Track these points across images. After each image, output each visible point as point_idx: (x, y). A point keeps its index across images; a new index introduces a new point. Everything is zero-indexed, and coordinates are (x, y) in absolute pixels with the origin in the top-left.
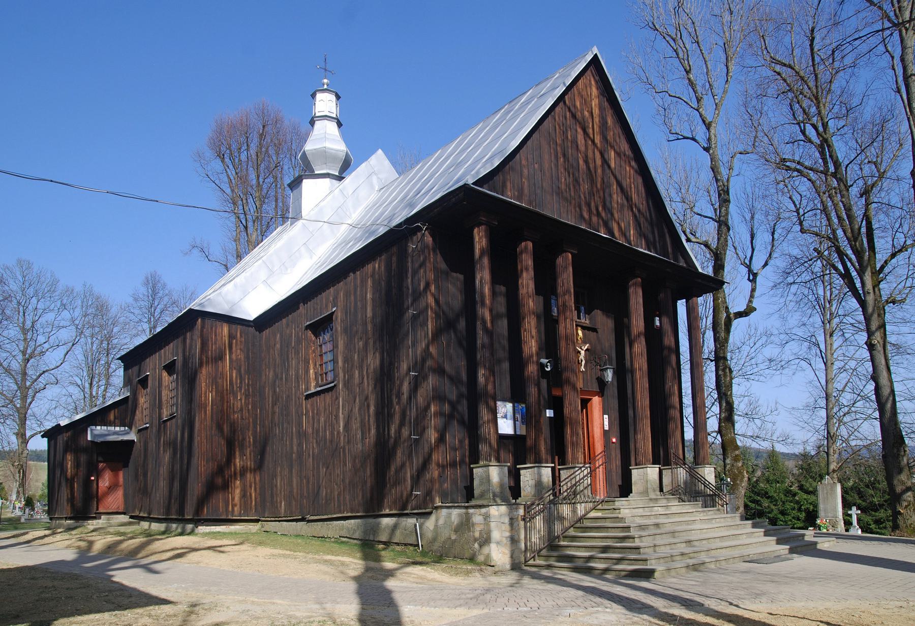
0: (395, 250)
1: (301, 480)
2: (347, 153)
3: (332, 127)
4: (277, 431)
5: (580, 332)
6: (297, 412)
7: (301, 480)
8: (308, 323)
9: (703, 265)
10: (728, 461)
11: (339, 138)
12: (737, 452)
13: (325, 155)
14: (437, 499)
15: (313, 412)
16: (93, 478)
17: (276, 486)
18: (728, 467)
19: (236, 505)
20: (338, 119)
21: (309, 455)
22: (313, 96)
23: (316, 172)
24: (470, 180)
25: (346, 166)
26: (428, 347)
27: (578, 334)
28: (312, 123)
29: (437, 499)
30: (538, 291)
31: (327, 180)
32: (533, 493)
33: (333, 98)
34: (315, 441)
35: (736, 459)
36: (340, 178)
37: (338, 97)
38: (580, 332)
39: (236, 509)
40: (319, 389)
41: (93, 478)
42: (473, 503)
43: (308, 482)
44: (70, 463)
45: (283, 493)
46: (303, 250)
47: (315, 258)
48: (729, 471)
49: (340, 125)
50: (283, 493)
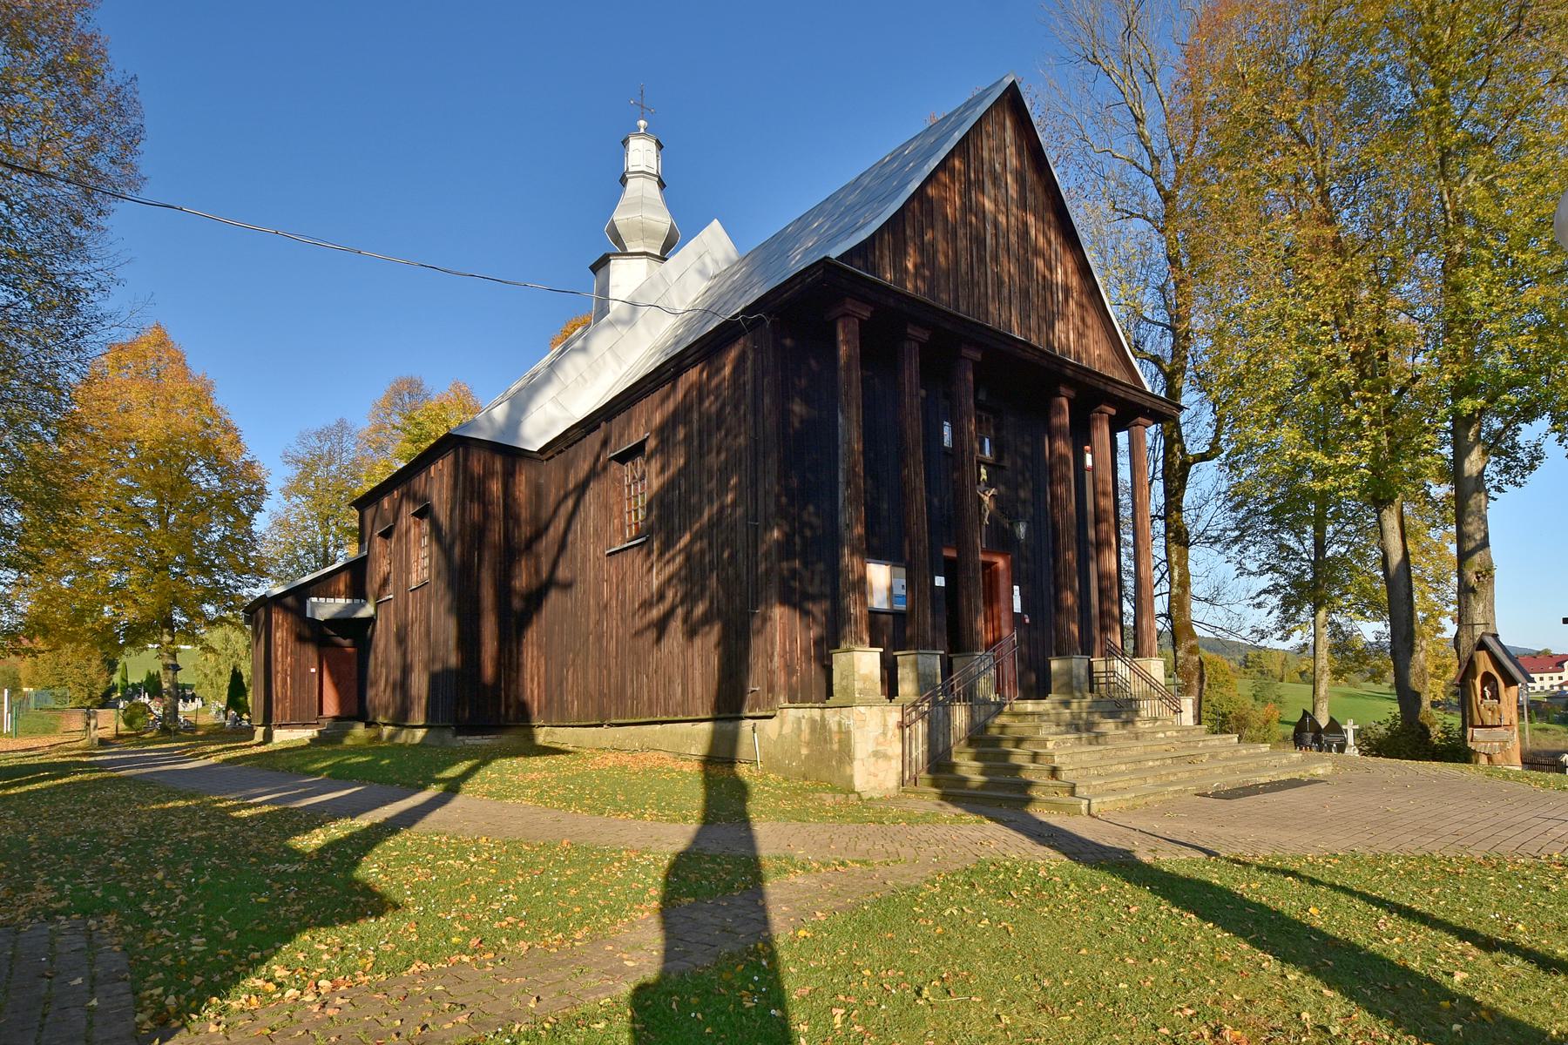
0: (1071, 556)
1: (600, 672)
2: (672, 225)
3: (652, 187)
4: (569, 605)
5: (983, 471)
6: (596, 577)
7: (600, 672)
8: (612, 455)
9: (1150, 381)
10: (1179, 654)
11: (662, 204)
12: (1193, 642)
13: (646, 232)
14: (782, 699)
15: (617, 577)
16: (313, 670)
17: (567, 679)
18: (1180, 662)
19: (511, 707)
20: (659, 178)
21: (612, 637)
22: (625, 142)
23: (629, 251)
24: (834, 253)
25: (670, 245)
26: (975, 398)
27: (979, 474)
28: (623, 181)
29: (782, 699)
30: (224, 760)
31: (644, 261)
32: (914, 691)
33: (653, 146)
34: (619, 617)
35: (1192, 650)
36: (663, 258)
37: (660, 146)
38: (983, 471)
39: (511, 712)
40: (626, 545)
41: (313, 670)
42: (830, 702)
43: (609, 674)
44: (280, 649)
45: (575, 689)
46: (608, 356)
47: (625, 368)
48: (1181, 667)
49: (662, 185)
50: (575, 689)
